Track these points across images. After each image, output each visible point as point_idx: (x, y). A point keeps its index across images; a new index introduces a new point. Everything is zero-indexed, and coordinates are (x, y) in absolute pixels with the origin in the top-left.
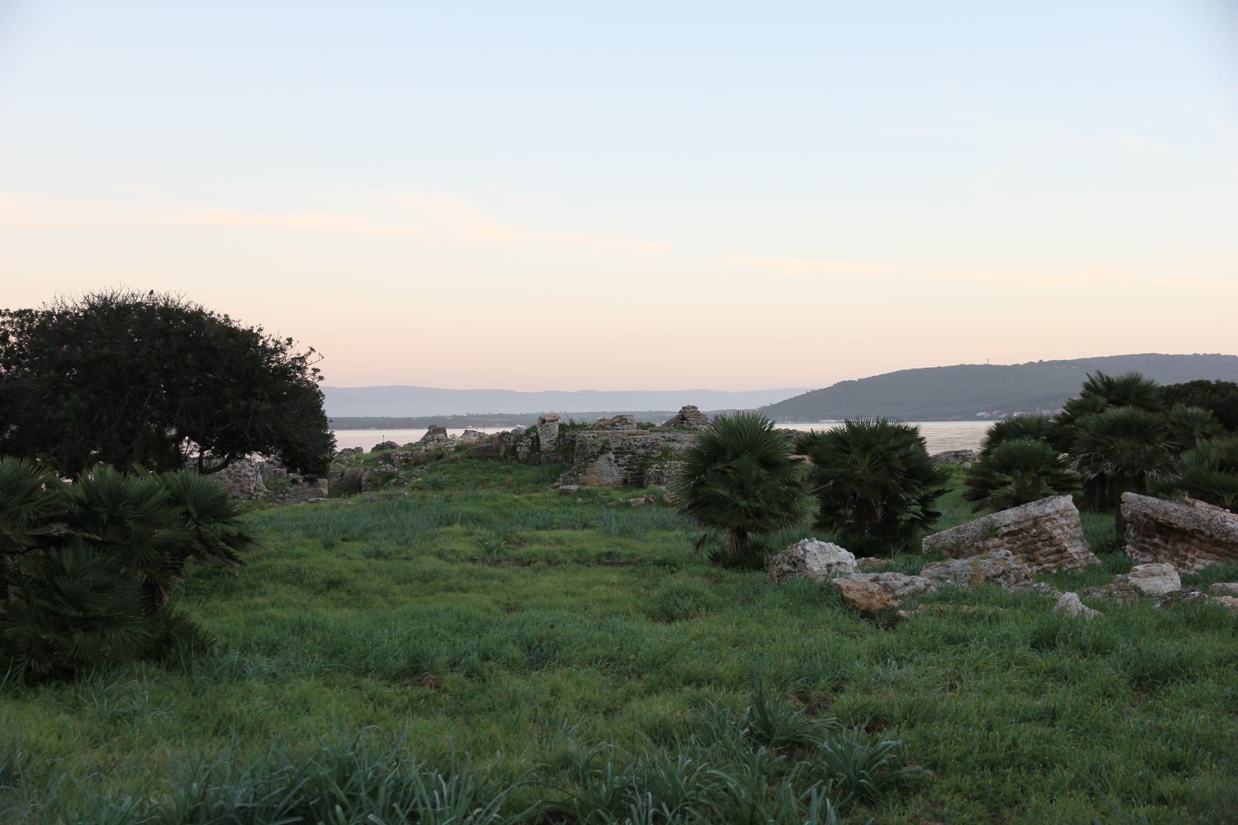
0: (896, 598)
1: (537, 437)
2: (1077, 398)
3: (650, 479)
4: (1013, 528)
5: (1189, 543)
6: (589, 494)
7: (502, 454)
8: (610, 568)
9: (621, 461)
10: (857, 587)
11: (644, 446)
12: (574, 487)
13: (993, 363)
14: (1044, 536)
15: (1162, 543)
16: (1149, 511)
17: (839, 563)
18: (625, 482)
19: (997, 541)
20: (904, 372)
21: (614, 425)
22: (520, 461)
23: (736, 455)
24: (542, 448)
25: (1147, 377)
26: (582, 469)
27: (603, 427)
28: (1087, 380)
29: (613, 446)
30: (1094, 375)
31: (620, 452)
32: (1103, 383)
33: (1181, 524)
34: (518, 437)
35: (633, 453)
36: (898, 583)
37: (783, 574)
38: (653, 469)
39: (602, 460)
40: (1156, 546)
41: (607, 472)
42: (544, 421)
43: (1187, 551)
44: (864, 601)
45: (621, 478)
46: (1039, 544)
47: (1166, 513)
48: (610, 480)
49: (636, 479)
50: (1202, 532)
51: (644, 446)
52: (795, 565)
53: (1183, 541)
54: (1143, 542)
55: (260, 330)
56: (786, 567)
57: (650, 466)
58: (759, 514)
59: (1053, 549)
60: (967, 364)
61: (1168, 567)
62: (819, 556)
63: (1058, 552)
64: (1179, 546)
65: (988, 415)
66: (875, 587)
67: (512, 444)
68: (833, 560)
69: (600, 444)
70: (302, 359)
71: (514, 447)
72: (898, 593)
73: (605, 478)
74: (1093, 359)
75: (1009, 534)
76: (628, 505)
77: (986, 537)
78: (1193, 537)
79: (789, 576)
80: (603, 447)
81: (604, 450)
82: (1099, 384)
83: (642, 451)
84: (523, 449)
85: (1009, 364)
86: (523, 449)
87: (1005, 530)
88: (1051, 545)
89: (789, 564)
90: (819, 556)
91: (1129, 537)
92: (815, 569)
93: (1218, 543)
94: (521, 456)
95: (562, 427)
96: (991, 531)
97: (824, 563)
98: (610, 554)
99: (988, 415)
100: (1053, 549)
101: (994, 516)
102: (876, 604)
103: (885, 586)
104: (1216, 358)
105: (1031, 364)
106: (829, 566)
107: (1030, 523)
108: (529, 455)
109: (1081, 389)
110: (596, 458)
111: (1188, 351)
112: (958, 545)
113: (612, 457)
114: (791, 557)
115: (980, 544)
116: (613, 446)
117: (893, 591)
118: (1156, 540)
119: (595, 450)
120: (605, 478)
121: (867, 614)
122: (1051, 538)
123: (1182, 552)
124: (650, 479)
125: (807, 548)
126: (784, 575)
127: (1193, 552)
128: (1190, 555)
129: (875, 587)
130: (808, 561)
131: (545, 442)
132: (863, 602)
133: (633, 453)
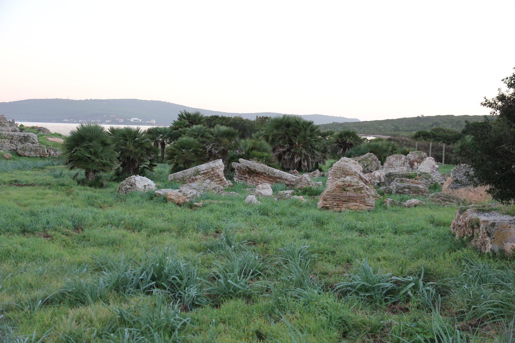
0: (188, 198)
2: (176, 120)
4: (205, 171)
5: (260, 177)
8: (30, 187)
10: (174, 194)
13: (71, 98)
14: (216, 175)
15: (249, 177)
16: (249, 166)
17: (148, 185)
19: (200, 176)
20: (30, 100)
23: (90, 141)
25: (202, 113)
28: (180, 113)
30: (183, 111)
32: (186, 114)
33: (259, 170)
36: (189, 193)
37: (127, 189)
40: (246, 178)
43: (259, 180)
44: (176, 199)
46: (214, 177)
47: (254, 166)
50: (265, 173)
52: (132, 186)
53: (257, 176)
54: (242, 176)
56: (128, 187)
58: (104, 165)
59: (219, 179)
61: (268, 185)
62: (141, 182)
63: (221, 180)
64: (255, 178)
65: (68, 121)
66: (180, 194)
68: (146, 184)
72: (188, 196)
74: (112, 100)
75: (204, 173)
77: (195, 175)
78: (261, 175)
79: (129, 190)
82: (184, 115)
87: (203, 172)
88: (218, 178)
90: (141, 182)
91: (236, 175)
92: (140, 187)
93: (271, 177)
96: (197, 173)
97: (143, 185)
98: (16, 181)
99: (68, 121)
100: (219, 179)
101: (198, 167)
102: (182, 201)
103: (184, 193)
104: (340, 118)
105: (87, 100)
106: (145, 186)
107: (211, 170)
109: (178, 117)
111: (111, 98)
112: (183, 178)
114: (130, 182)
115: (194, 178)
117: (187, 195)
118: (246, 176)
121: (179, 204)
122: (218, 175)
123: (256, 180)
125: (136, 179)
126: (127, 190)
127: (262, 180)
128: (260, 181)
129: (180, 194)
130: (136, 184)
132: (177, 200)
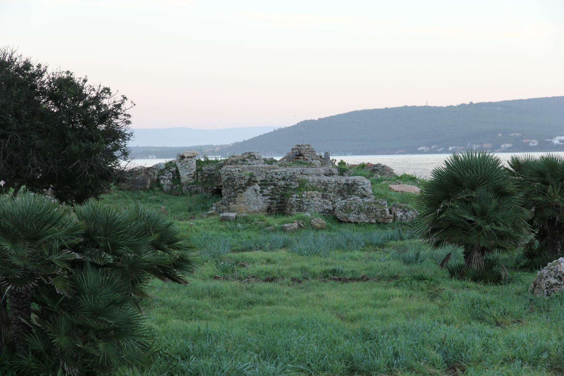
1: (177, 171)
3: (293, 207)
6: (246, 220)
7: (148, 186)
9: (266, 192)
11: (284, 179)
12: (233, 215)
13: (432, 104)
18: (269, 209)
21: (244, 160)
22: (165, 192)
24: (183, 181)
26: (232, 199)
27: (236, 162)
29: (259, 179)
31: (264, 184)
34: (161, 171)
35: (275, 185)
37: (550, 286)
38: (293, 199)
39: (249, 191)
41: (253, 201)
42: (183, 157)
45: (265, 206)
48: (256, 208)
49: (279, 206)
51: (284, 179)
55: (85, 81)
56: (553, 281)
57: (290, 196)
58: (502, 236)
60: (409, 105)
65: (428, 149)
67: (156, 177)
69: (247, 177)
70: (119, 106)
71: (158, 180)
73: (252, 206)
74: (514, 101)
76: (283, 230)
79: (555, 288)
80: (250, 179)
81: (251, 182)
83: (282, 183)
84: (166, 182)
85: (444, 105)
86: (166, 182)
89: (555, 278)
94: (165, 187)
95: (199, 162)
98: (334, 272)
99: (428, 149)
108: (172, 187)
110: (244, 189)
113: (258, 188)
114: (556, 272)
116: (259, 179)
119: (243, 182)
120: (252, 206)
124: (293, 207)
131: (185, 176)
133: (275, 185)
